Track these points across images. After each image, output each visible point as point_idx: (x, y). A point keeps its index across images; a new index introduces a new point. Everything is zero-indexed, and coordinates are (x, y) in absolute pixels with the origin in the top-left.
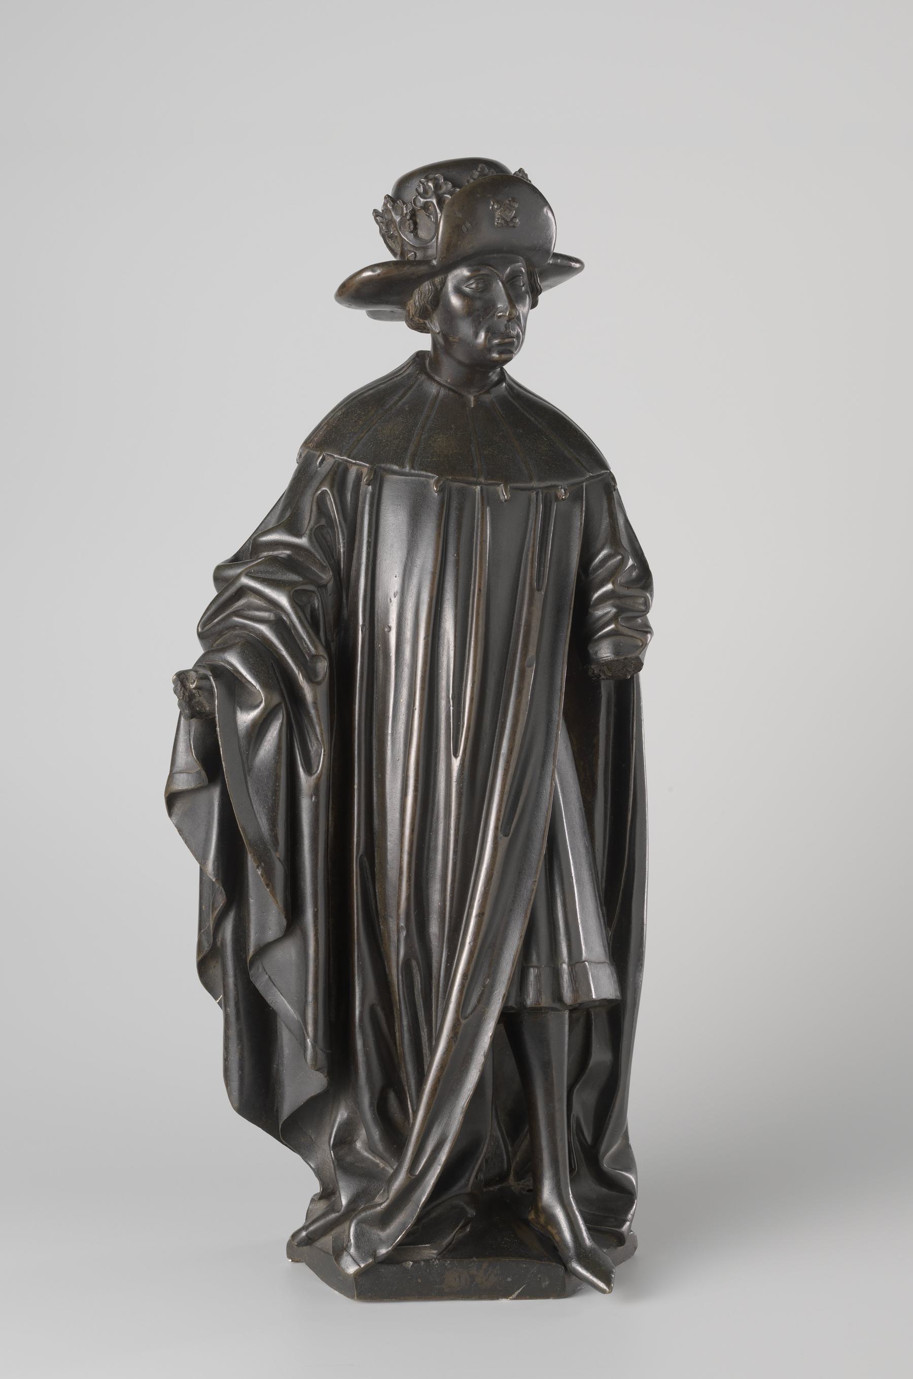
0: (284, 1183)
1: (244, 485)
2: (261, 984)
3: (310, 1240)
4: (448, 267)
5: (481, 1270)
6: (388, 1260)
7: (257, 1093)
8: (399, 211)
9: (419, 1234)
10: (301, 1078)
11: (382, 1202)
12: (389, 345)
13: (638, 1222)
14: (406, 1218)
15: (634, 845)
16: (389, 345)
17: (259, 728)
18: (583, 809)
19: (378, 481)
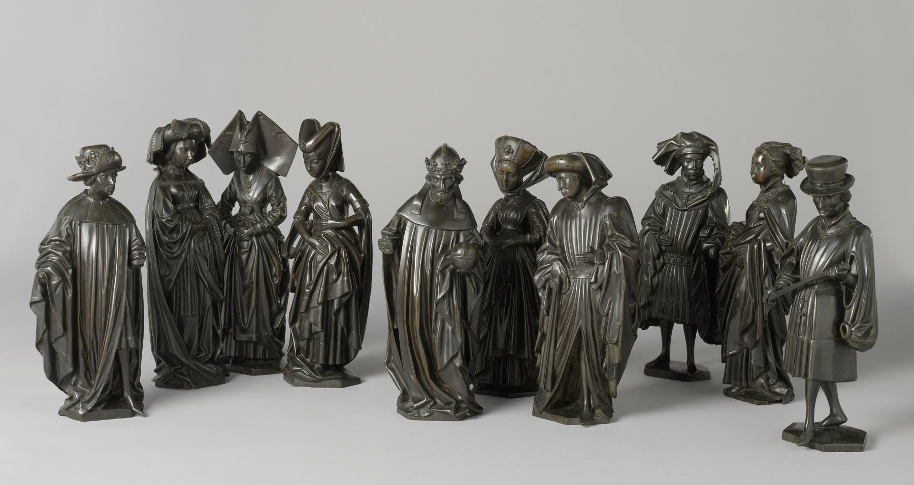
0: (59, 397)
1: (44, 222)
2: (54, 346)
3: (68, 409)
4: (97, 173)
5: (111, 411)
6: (90, 411)
7: (53, 375)
8: (82, 160)
9: (96, 406)
10: (66, 367)
11: (87, 398)
12: (80, 187)
13: (145, 402)
14: (94, 402)
15: (85, 305)
16: (80, 187)
17: (57, 285)
18: (561, 418)
19: (80, 225)
